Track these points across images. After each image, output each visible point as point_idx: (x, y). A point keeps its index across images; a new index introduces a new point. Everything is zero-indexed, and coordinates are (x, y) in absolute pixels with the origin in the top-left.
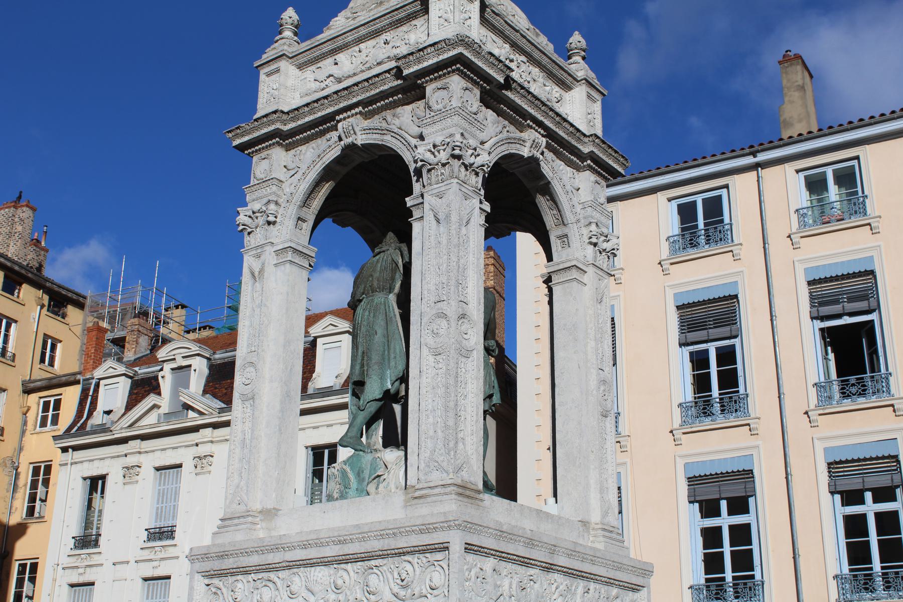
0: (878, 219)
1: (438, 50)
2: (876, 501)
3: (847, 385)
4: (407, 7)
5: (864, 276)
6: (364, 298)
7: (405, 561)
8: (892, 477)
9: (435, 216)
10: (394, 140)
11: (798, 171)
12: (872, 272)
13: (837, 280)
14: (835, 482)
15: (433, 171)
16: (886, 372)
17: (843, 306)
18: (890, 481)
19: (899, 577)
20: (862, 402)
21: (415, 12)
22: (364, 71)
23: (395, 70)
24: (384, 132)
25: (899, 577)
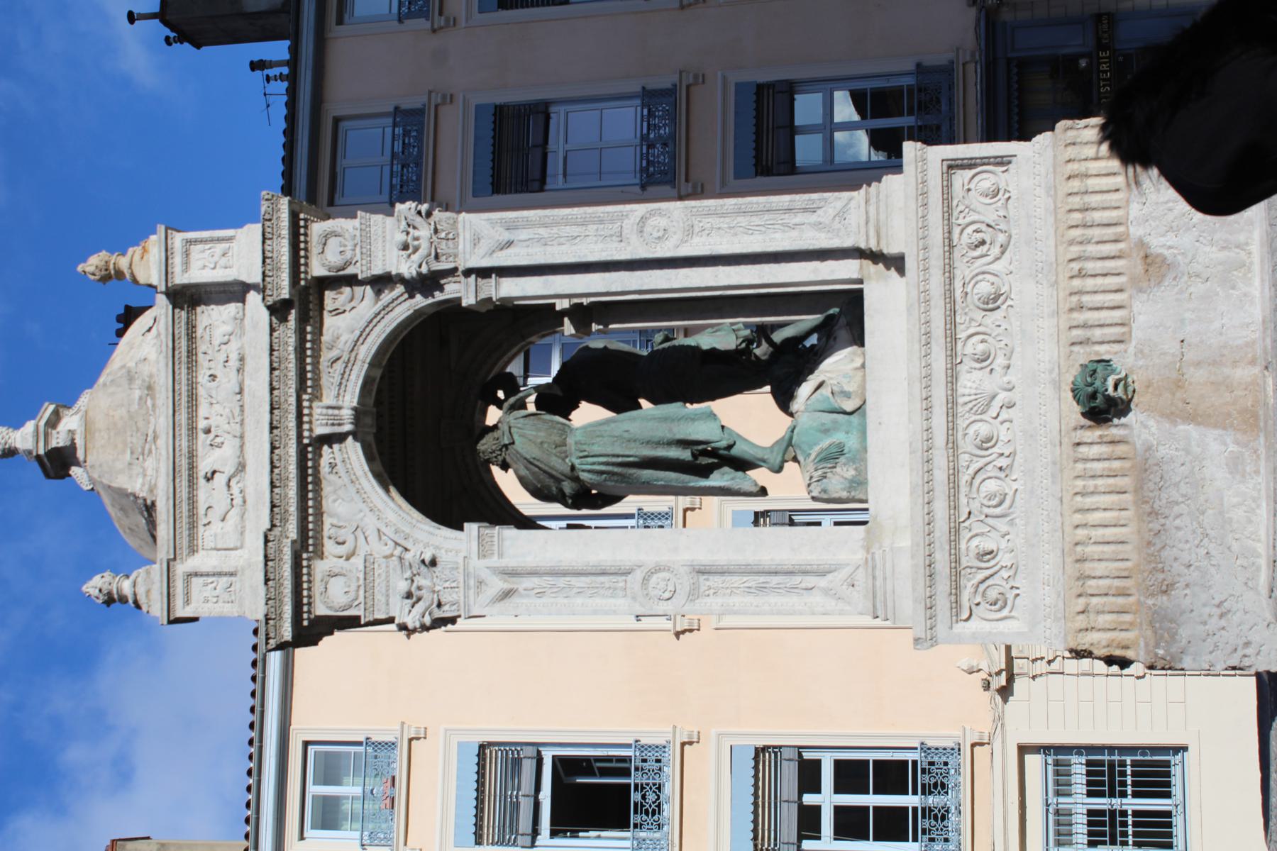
0: (406, 726)
1: (273, 234)
2: (817, 790)
3: (642, 806)
4: (176, 332)
5: (484, 760)
6: (570, 461)
7: (960, 239)
8: (785, 760)
9: (502, 249)
10: (370, 339)
11: (302, 838)
12: (482, 747)
13: (483, 802)
14: (783, 843)
15: (439, 251)
16: (633, 749)
17: (524, 796)
18: (792, 763)
19: (929, 769)
20: (671, 789)
21: (188, 323)
22: (242, 420)
23: (273, 318)
24: (352, 359)
25: (929, 769)
